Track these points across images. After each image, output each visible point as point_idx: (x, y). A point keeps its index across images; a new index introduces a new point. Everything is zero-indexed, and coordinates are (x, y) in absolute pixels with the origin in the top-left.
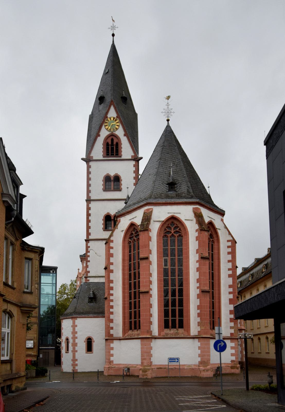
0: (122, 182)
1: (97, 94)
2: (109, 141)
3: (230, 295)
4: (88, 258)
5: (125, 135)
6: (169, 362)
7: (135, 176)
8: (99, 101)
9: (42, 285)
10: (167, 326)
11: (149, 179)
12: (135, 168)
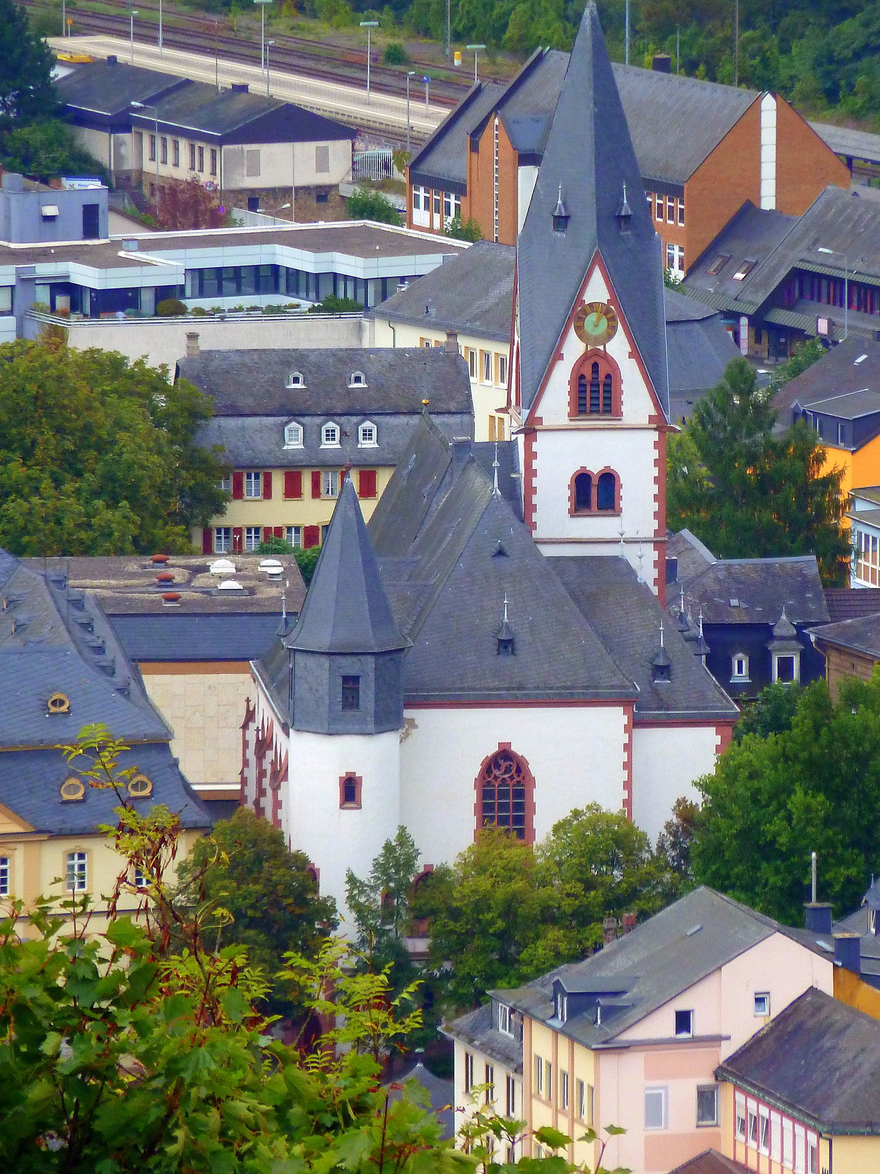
1: (357, 734)
5: (631, 355)
6: (663, 1092)
7: (657, 475)
8: (294, 849)
9: (236, 783)
12: (657, 504)
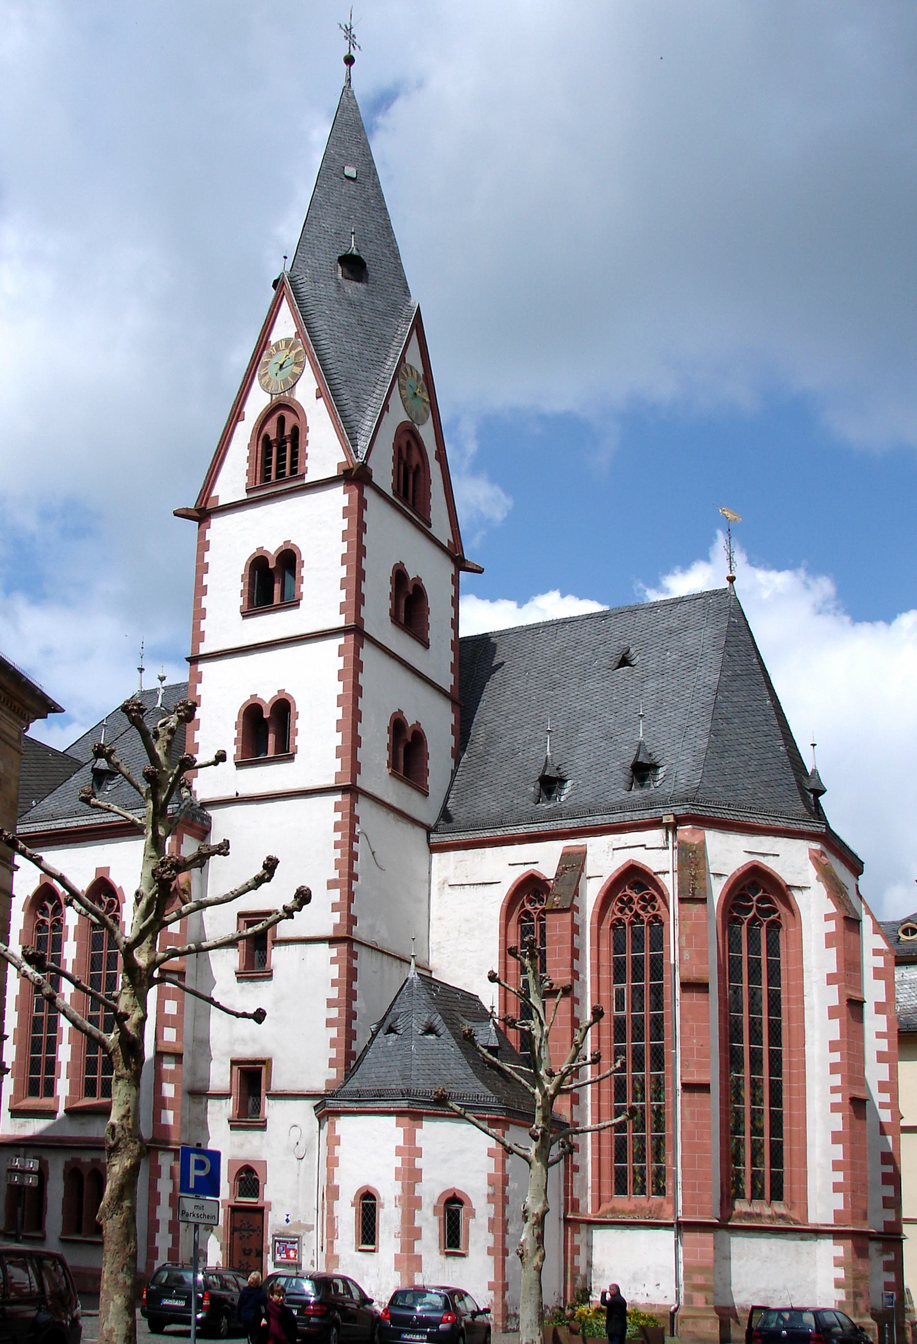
0: (304, 572)
2: (271, 429)
3: (107, 866)
4: (335, 955)
10: (621, 1189)
11: (317, 292)
